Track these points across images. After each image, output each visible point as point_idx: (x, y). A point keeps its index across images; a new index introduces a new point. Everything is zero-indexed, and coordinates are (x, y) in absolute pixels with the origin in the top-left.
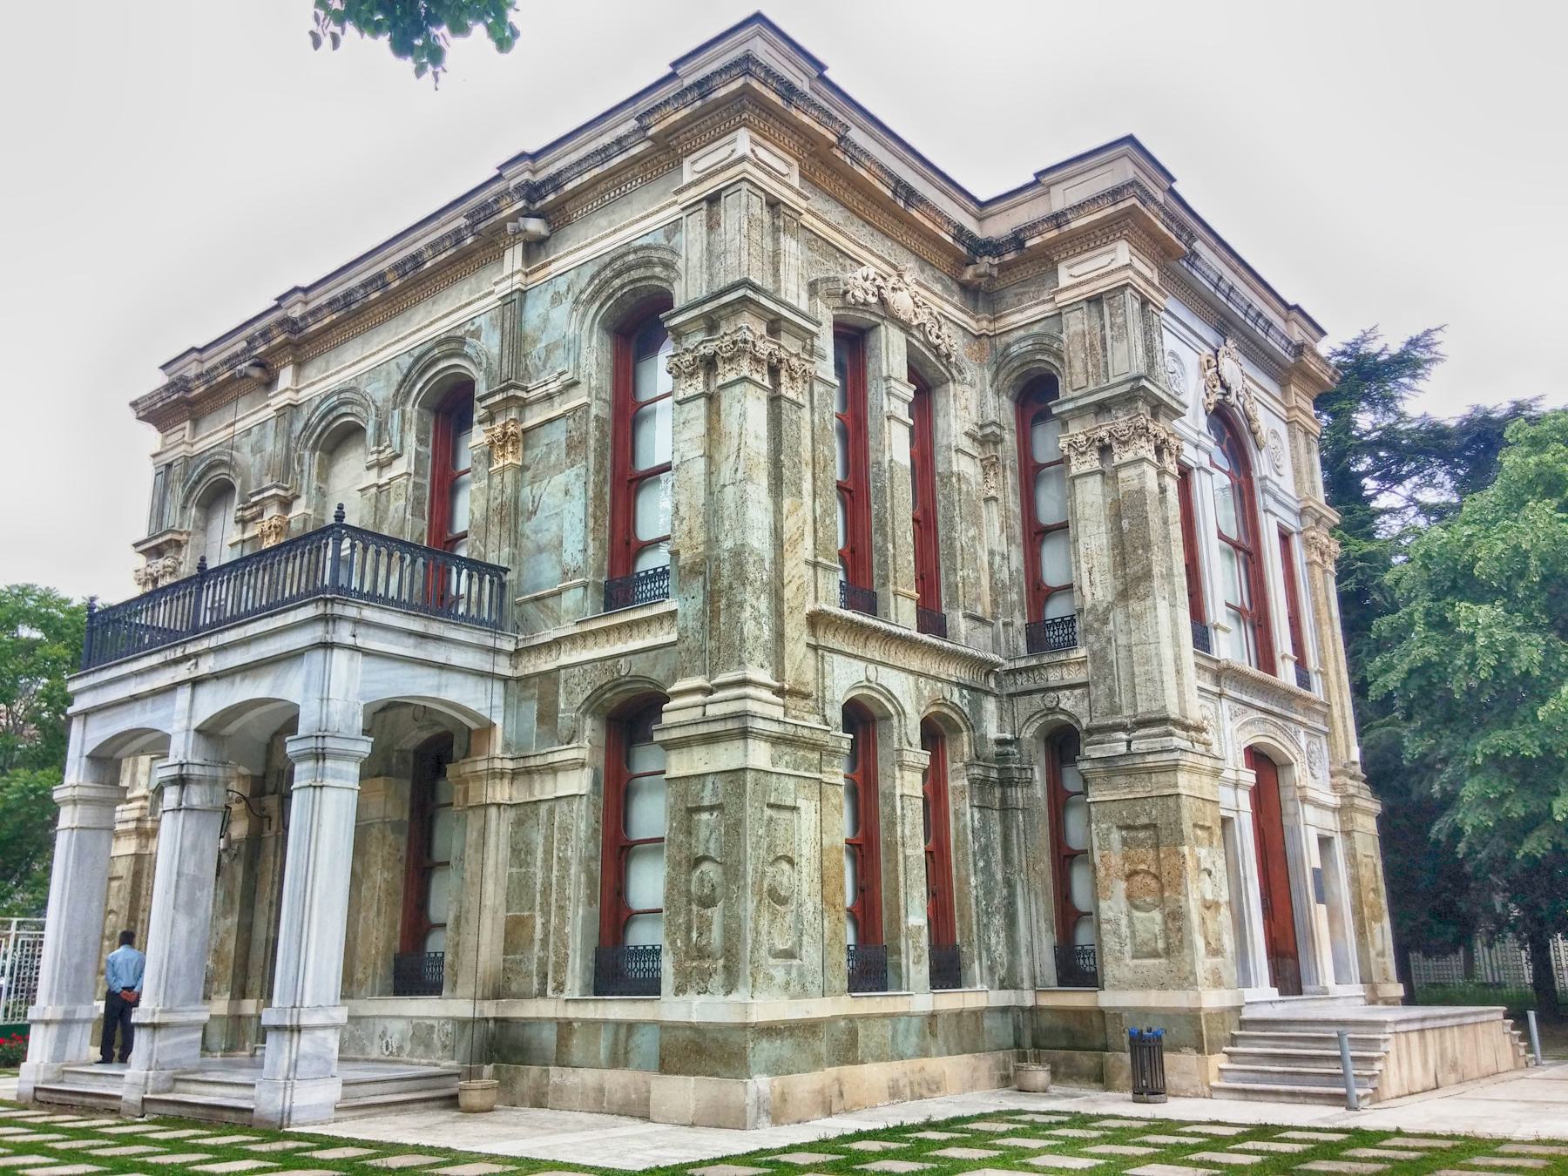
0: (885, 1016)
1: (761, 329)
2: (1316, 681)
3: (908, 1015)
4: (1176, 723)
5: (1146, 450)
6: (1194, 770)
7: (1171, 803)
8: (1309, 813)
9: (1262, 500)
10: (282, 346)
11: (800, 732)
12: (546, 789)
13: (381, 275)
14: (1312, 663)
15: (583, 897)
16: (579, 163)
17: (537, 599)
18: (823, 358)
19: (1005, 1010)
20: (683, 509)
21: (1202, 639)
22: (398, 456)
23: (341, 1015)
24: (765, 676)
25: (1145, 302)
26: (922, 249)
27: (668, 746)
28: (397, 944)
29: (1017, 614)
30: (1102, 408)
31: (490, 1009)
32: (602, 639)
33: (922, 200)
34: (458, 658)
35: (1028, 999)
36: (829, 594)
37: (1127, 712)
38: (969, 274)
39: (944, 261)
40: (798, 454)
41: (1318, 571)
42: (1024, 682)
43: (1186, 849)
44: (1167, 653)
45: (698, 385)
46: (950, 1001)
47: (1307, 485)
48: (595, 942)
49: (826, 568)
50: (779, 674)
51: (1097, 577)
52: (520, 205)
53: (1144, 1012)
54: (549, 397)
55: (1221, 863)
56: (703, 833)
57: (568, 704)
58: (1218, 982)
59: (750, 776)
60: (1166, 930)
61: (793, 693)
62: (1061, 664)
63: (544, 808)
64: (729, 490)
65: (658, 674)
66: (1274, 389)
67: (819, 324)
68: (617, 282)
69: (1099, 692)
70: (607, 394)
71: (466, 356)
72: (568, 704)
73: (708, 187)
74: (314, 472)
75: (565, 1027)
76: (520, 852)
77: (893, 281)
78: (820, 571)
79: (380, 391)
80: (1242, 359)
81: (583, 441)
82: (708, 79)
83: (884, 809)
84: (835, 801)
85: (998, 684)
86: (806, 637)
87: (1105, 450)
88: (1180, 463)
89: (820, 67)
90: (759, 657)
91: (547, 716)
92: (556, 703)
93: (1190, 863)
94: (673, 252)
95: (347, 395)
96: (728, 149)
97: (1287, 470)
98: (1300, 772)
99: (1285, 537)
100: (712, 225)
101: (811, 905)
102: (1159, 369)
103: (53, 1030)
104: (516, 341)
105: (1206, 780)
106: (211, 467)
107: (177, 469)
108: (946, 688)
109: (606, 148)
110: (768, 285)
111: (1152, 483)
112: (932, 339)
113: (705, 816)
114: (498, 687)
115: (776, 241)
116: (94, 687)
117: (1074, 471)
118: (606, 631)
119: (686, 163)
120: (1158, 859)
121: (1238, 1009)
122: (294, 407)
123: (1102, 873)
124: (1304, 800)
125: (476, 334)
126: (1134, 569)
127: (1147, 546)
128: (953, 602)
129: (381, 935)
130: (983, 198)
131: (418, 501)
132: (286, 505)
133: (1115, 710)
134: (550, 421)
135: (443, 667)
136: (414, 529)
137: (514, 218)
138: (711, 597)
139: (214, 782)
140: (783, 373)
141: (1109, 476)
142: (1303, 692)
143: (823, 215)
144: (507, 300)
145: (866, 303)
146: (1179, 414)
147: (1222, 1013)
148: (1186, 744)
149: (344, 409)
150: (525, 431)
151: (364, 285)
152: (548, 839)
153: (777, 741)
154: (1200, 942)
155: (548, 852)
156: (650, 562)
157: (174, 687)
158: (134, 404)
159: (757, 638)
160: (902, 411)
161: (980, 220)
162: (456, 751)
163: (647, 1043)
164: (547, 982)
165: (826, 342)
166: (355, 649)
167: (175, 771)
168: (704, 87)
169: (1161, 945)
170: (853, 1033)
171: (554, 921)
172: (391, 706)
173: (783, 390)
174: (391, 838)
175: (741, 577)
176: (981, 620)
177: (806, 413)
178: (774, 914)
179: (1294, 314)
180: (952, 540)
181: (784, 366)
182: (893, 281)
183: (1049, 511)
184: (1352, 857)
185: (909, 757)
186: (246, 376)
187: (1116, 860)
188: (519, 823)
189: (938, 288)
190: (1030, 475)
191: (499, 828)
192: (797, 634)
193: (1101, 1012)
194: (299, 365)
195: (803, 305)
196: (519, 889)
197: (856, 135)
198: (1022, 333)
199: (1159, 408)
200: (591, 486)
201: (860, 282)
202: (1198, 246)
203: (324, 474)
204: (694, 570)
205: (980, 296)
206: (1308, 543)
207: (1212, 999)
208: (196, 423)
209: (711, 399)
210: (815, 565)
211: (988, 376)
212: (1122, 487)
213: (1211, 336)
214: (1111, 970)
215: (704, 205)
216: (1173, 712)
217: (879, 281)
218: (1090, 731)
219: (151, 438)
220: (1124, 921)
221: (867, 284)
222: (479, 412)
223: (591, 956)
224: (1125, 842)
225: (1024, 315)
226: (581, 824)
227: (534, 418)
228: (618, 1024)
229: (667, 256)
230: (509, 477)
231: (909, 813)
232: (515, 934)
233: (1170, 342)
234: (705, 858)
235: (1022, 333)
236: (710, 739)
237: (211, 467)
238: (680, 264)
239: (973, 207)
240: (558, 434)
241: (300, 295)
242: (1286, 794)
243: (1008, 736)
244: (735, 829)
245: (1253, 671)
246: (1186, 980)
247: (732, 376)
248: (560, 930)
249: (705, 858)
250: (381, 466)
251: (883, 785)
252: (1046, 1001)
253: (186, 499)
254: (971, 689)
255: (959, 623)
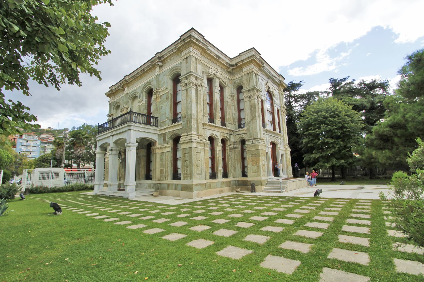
0: (215, 182)
1: (194, 79)
2: (282, 132)
3: (219, 182)
4: (259, 139)
5: (256, 97)
6: (262, 145)
7: (258, 150)
8: (280, 151)
9: (274, 105)
10: (125, 84)
11: (201, 141)
12: (164, 150)
13: (139, 72)
14: (282, 129)
15: (170, 166)
16: (167, 53)
17: (163, 122)
18: (205, 83)
19: (235, 181)
20: (183, 108)
21: (264, 126)
22: (142, 101)
23: (135, 183)
24: (195, 133)
25: (256, 74)
26: (221, 66)
27: (181, 144)
28: (146, 173)
29: (237, 123)
30: (249, 91)
31: (158, 182)
32: (172, 128)
33: (221, 58)
34: (150, 131)
35: (237, 179)
36: (206, 121)
37: (252, 137)
38: (229, 70)
39: (225, 68)
40: (200, 98)
41: (283, 115)
42: (238, 133)
43: (260, 157)
44: (258, 128)
45: (185, 88)
46: (226, 180)
47: (282, 102)
48: (172, 173)
49: (206, 116)
50: (198, 133)
51: (248, 117)
52: (158, 60)
53: (254, 181)
54: (163, 91)
55: (266, 159)
56: (186, 157)
57: (167, 138)
58: (264, 176)
59: (193, 148)
60: (257, 169)
61: (200, 135)
62: (243, 130)
63: (164, 153)
64: (189, 104)
65: (180, 133)
66: (277, 88)
67: (204, 78)
68: (173, 72)
69: (248, 134)
70: (172, 90)
71: (151, 85)
72: (167, 138)
73: (186, 57)
74: (131, 103)
75: (169, 185)
76: (161, 160)
77: (216, 71)
78: (204, 117)
79: (139, 91)
80: (272, 83)
81: (168, 98)
82: (185, 39)
83: (215, 152)
84: (207, 151)
85: (234, 133)
86: (202, 127)
87: (250, 97)
88: (261, 99)
89: (204, 37)
90: (194, 130)
91: (164, 140)
92: (165, 138)
93: (261, 159)
94: (181, 67)
95: (135, 92)
96: (188, 50)
97: (279, 100)
98: (279, 145)
99: (278, 110)
100: (186, 63)
101: (203, 167)
102: (258, 85)
103: (98, 185)
104: (158, 82)
105: (264, 147)
106: (117, 103)
107: (112, 104)
108: (225, 134)
109: (170, 51)
110: (195, 72)
111: (256, 102)
112: (223, 80)
113: (187, 154)
114: (157, 135)
115: (197, 65)
116: (100, 136)
117: (245, 101)
118: (172, 127)
119: (182, 53)
120: (256, 159)
121: (268, 180)
122: (127, 94)
123: (248, 161)
124: (279, 149)
125: (153, 81)
126: (253, 116)
127: (255, 112)
128: (227, 121)
129: (143, 172)
130: (231, 58)
131: (145, 108)
132: (127, 108)
133: (250, 137)
134: (164, 94)
135: (148, 132)
136: (145, 112)
137: (157, 63)
138: (187, 121)
139: (116, 150)
140: (198, 86)
141: (250, 101)
142: (280, 133)
143: (204, 60)
144: (157, 76)
145: (212, 75)
146: (261, 92)
147: (265, 180)
148: (261, 142)
149: (134, 94)
150: (160, 96)
151: (136, 74)
152: (165, 157)
153: (198, 143)
154: (262, 170)
155: (165, 160)
156: (179, 116)
157: (110, 136)
158: (105, 94)
159: (194, 127)
160: (218, 92)
161: (231, 61)
162: (152, 145)
163: (179, 187)
164: (166, 177)
165: (205, 81)
166: (134, 130)
167: (111, 149)
168: (184, 40)
169: (256, 171)
170: (210, 185)
171: (166, 170)
172: (143, 139)
173: (198, 89)
174: (144, 158)
175: (191, 118)
176: (231, 124)
177: (202, 92)
178: (197, 168)
179: (280, 76)
180: (226, 111)
181: (198, 85)
182: (216, 71)
183: (241, 108)
184: (286, 157)
185: (219, 145)
186: (120, 89)
187: (250, 159)
188: (161, 156)
189: (224, 72)
190: (239, 101)
191: (158, 156)
192: (201, 126)
193: (248, 181)
194: (128, 87)
195: (201, 75)
196: (162, 165)
197: (209, 48)
198: (237, 79)
199: (258, 90)
200: (170, 105)
201: (211, 72)
202: (264, 65)
203: (132, 104)
204: (185, 117)
205: (231, 73)
206: (281, 111)
207: (263, 178)
208: (114, 96)
209: (187, 90)
210: (204, 116)
211: (232, 86)
212: (252, 103)
213: (267, 79)
214: (249, 175)
215: (185, 59)
216: (259, 137)
217: (214, 71)
218: (247, 140)
219: (108, 99)
220: (251, 168)
221: (212, 72)
222: (153, 94)
223: (172, 175)
224: (252, 156)
225: (237, 76)
226: (170, 156)
227: (161, 94)
228: (176, 184)
229: (180, 68)
230: (158, 103)
231: (219, 153)
232: (161, 171)
233: (260, 80)
234: (187, 160)
235: (237, 79)
236: (187, 143)
237: (117, 103)
238: (182, 69)
239: (230, 59)
240: (165, 97)
241: (127, 76)
242: (277, 149)
243: (235, 141)
244: (191, 156)
245: (273, 131)
246: (260, 176)
247: (189, 87)
248: (167, 171)
249: (187, 160)
250: (140, 102)
251: (215, 149)
252: (240, 179)
253: (114, 108)
254: (229, 134)
255: (227, 124)
